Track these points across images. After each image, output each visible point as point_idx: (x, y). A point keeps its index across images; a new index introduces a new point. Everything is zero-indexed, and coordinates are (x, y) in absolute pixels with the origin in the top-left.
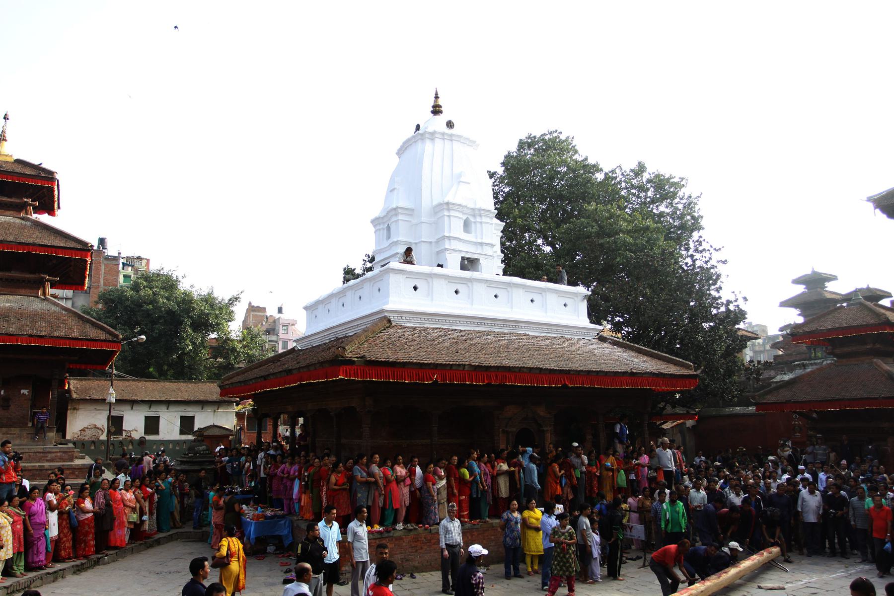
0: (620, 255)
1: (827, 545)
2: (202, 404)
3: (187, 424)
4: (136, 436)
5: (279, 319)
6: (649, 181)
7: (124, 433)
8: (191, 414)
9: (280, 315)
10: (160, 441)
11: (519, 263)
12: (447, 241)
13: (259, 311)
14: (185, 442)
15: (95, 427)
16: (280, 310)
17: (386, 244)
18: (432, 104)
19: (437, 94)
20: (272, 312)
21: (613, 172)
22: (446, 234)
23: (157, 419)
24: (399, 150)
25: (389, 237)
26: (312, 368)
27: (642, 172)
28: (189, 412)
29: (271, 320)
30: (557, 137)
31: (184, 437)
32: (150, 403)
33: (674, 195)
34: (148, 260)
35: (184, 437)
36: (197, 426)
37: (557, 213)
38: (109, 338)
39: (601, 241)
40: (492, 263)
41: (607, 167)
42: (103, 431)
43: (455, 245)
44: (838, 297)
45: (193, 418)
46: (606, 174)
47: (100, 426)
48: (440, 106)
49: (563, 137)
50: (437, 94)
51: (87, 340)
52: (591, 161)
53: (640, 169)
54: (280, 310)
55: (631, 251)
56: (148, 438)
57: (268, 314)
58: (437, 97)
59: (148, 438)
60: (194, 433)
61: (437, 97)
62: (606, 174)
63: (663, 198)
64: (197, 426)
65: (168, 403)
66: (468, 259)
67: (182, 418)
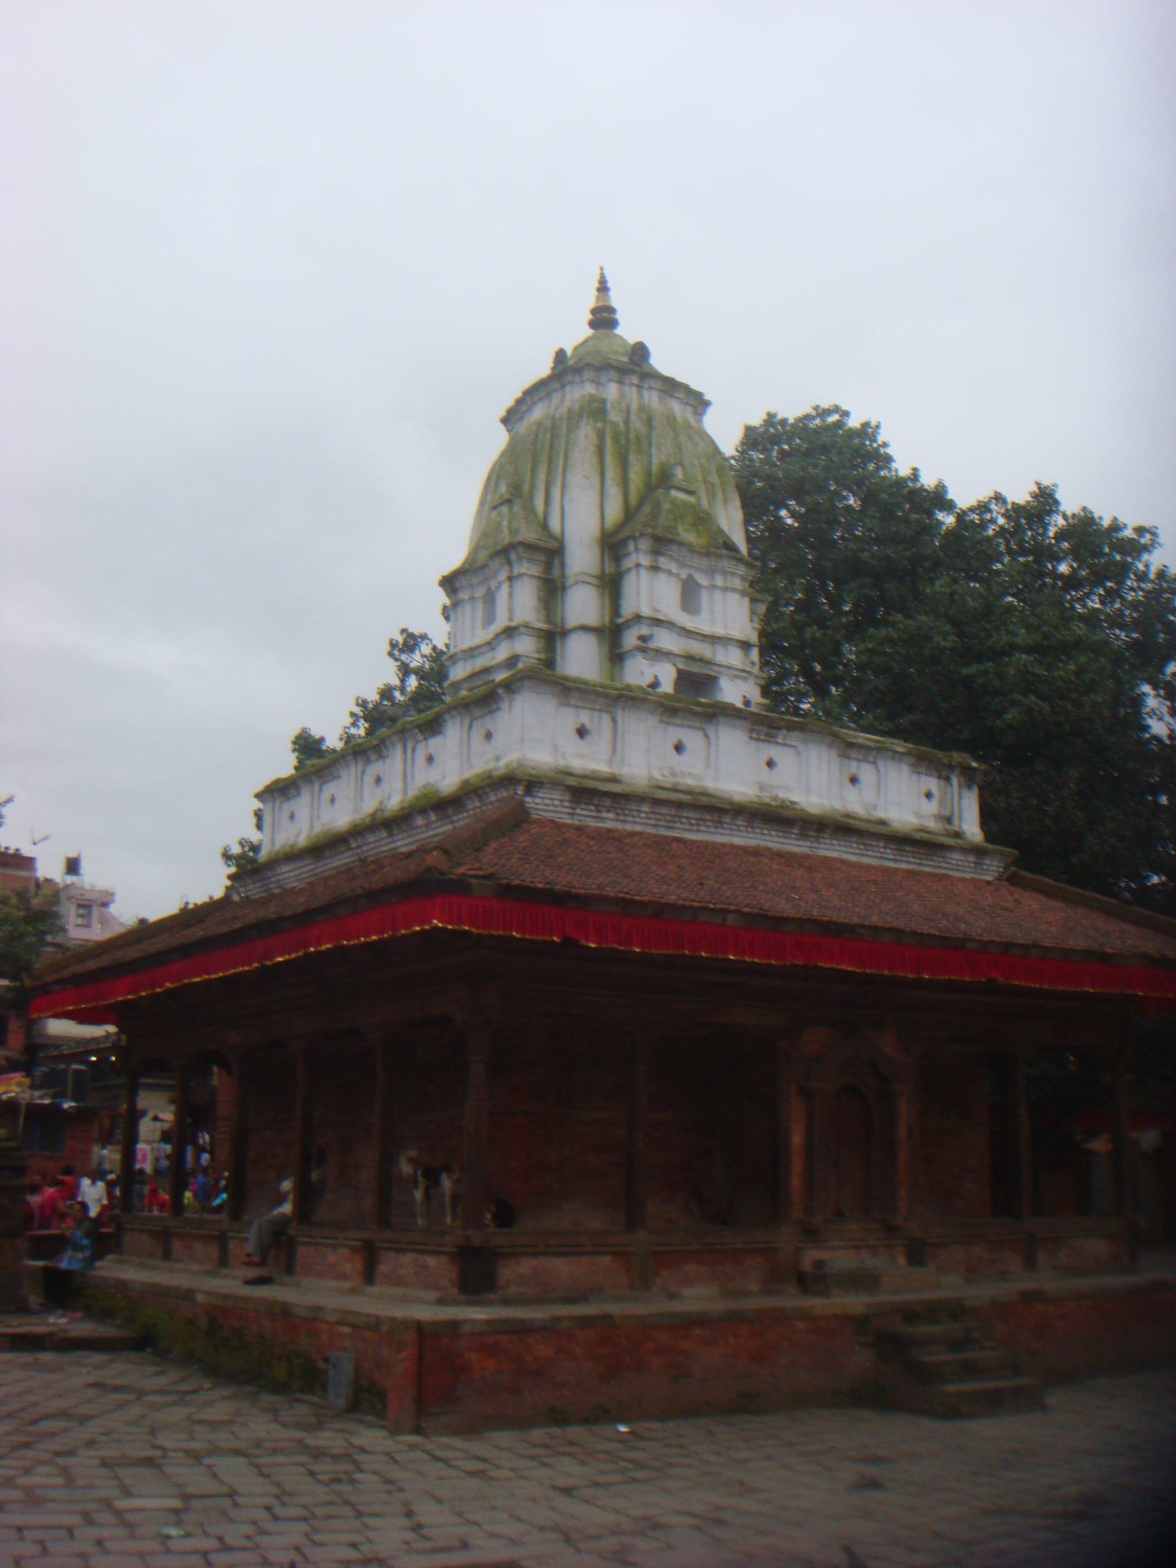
0: (1014, 703)
5: (67, 887)
6: (1061, 536)
9: (70, 879)
16: (73, 866)
17: (482, 635)
20: (49, 868)
21: (983, 508)
22: (646, 611)
24: (510, 412)
26: (636, 839)
27: (1050, 513)
29: (47, 891)
30: (839, 425)
33: (1123, 570)
37: (1084, 509)
39: (965, 671)
41: (964, 496)
46: (961, 517)
48: (592, 324)
49: (854, 422)
52: (928, 481)
53: (1045, 499)
54: (73, 866)
55: (1039, 695)
58: (603, 288)
61: (603, 288)
62: (961, 517)
63: (1098, 578)
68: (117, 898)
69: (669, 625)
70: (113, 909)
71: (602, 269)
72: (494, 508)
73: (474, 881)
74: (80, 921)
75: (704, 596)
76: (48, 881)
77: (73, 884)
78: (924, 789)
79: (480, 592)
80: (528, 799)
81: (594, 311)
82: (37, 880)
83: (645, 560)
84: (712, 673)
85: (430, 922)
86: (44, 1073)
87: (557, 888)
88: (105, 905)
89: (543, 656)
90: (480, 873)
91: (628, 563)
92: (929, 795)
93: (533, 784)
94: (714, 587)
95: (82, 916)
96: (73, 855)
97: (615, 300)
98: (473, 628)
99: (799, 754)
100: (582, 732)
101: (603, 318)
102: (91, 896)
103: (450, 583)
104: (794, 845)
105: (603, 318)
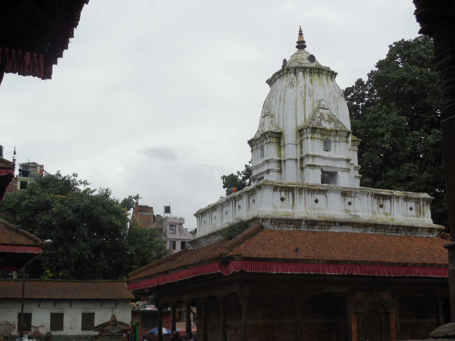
1: (128, 224)
2: (101, 302)
3: (88, 320)
4: (43, 331)
7: (33, 329)
8: (91, 311)
9: (168, 215)
10: (64, 336)
11: (377, 174)
12: (310, 159)
13: (146, 211)
14: (86, 337)
15: (8, 324)
16: (167, 210)
17: (260, 161)
18: (297, 40)
19: (300, 29)
20: (158, 211)
22: (310, 153)
23: (61, 316)
25: (263, 155)
28: (90, 309)
31: (85, 333)
32: (55, 301)
34: (42, 166)
35: (85, 333)
36: (97, 322)
38: (31, 242)
40: (348, 179)
42: (14, 328)
43: (318, 162)
44: (219, 237)
45: (93, 314)
47: (11, 323)
48: (297, 47)
50: (300, 29)
51: (13, 245)
54: (167, 210)
56: (54, 333)
57: (155, 213)
58: (301, 34)
59: (54, 333)
60: (96, 329)
61: (301, 34)
64: (97, 322)
65: (71, 301)
66: (327, 172)
67: (84, 315)
68: (185, 221)
69: (319, 157)
70: (184, 226)
71: (300, 27)
72: (263, 117)
73: (235, 257)
74: (171, 231)
75: (332, 145)
76: (158, 216)
77: (167, 217)
78: (409, 207)
79: (260, 146)
80: (263, 223)
81: (298, 42)
82: (154, 216)
83: (309, 135)
84: (335, 171)
85: (217, 271)
86: (152, 298)
87: (261, 256)
88: (181, 224)
89: (278, 169)
90: (237, 253)
91: (305, 136)
92: (411, 209)
93: (264, 220)
94: (336, 141)
95: (172, 229)
96: (168, 205)
97: (305, 38)
98: (258, 158)
99: (360, 199)
100: (282, 199)
101: (301, 45)
102: (175, 221)
103: (251, 143)
104: (357, 231)
105: (301, 45)
